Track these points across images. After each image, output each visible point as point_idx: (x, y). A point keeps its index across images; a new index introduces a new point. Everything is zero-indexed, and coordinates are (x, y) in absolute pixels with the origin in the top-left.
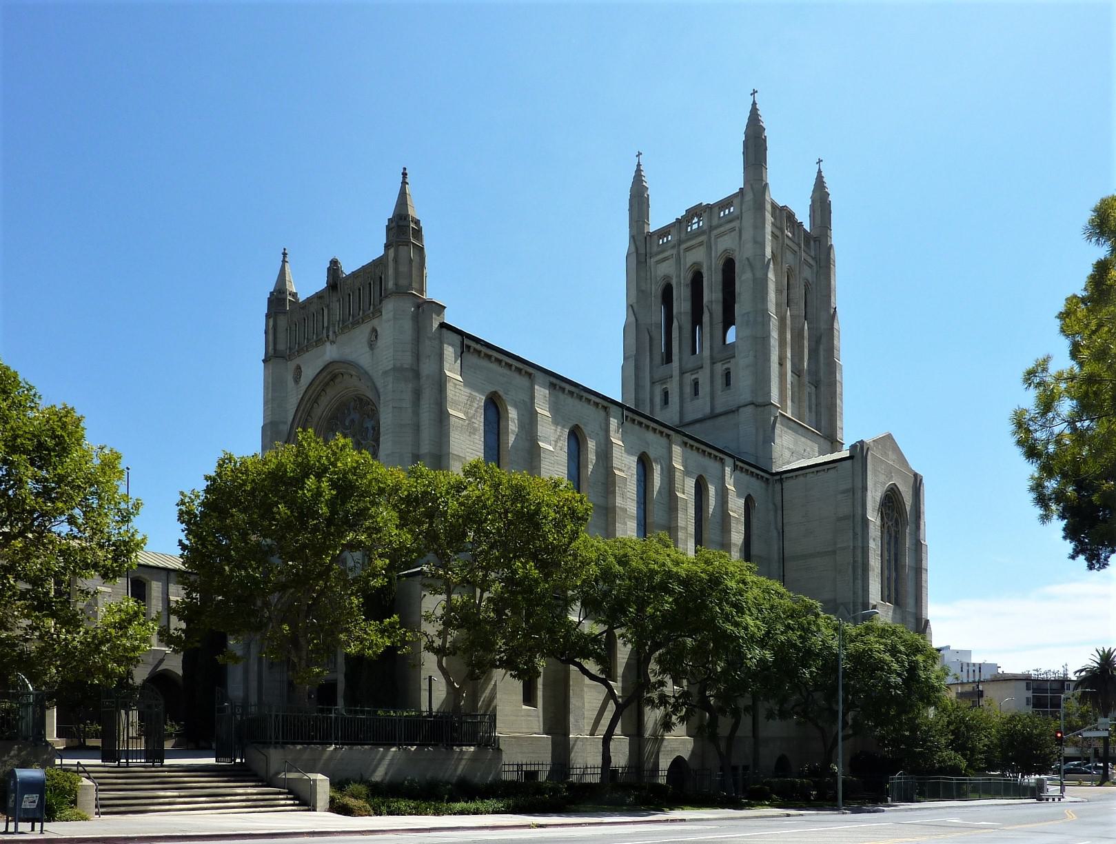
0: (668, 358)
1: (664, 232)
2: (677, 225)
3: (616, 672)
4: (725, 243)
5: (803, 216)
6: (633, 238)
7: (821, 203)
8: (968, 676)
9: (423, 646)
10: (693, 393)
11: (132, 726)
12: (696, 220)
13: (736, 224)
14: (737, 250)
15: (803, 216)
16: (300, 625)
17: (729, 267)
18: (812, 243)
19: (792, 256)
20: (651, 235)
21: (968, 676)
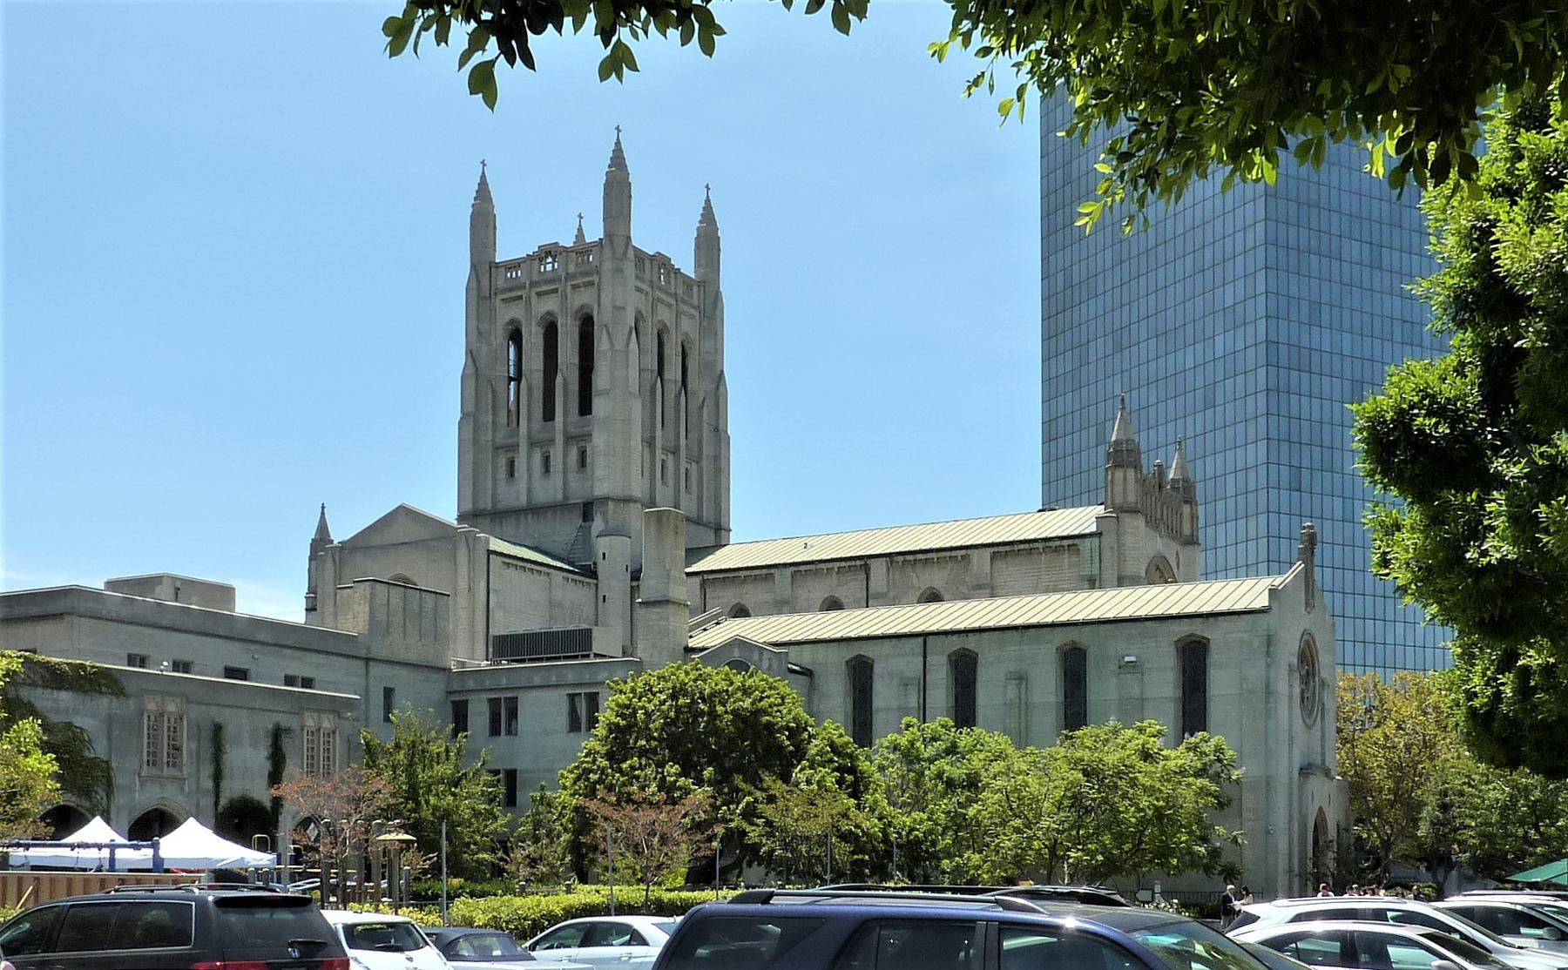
0: (549, 415)
1: (513, 265)
2: (528, 261)
3: (586, 699)
4: (584, 298)
5: (686, 263)
6: (474, 267)
7: (708, 242)
8: (1125, 479)
9: (134, 856)
10: (543, 470)
11: (152, 891)
12: (550, 260)
13: (595, 278)
14: (596, 306)
15: (686, 263)
16: (1392, 26)
17: (587, 326)
18: (695, 289)
19: (667, 309)
20: (497, 266)
21: (1125, 479)
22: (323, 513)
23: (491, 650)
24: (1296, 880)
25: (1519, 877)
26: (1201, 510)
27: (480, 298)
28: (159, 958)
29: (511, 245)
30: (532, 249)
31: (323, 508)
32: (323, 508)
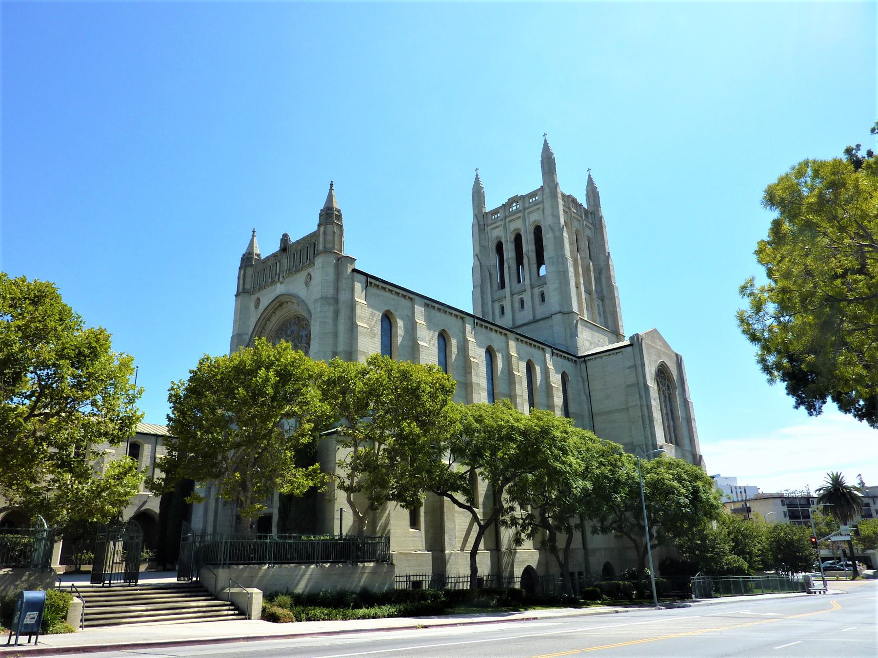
1: (495, 212)
2: (503, 208)
4: (534, 217)
6: (475, 216)
7: (593, 193)
12: (515, 204)
13: (540, 206)
18: (589, 215)
19: (578, 223)
20: (487, 214)
22: (331, 189)
23: (580, 270)
24: (476, 528)
25: (296, 582)
26: (630, 404)
27: (480, 230)
28: (339, 654)
29: (490, 205)
30: (505, 201)
31: (332, 185)
32: (332, 185)
